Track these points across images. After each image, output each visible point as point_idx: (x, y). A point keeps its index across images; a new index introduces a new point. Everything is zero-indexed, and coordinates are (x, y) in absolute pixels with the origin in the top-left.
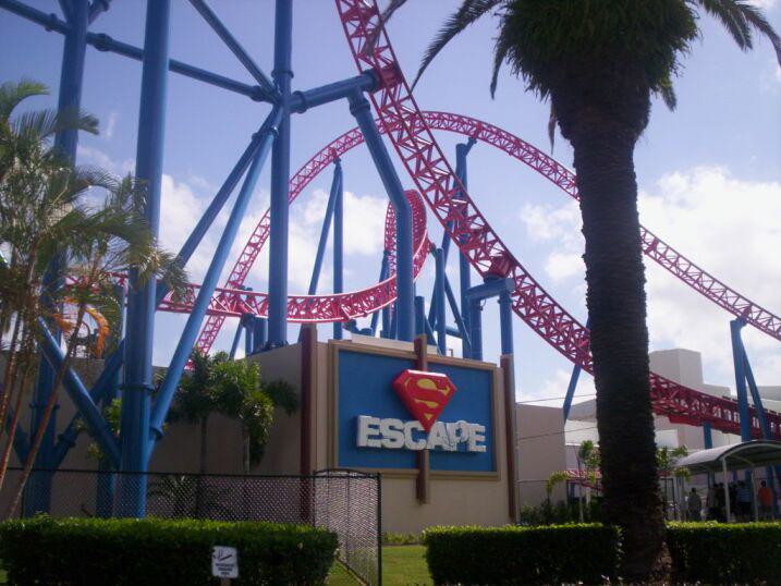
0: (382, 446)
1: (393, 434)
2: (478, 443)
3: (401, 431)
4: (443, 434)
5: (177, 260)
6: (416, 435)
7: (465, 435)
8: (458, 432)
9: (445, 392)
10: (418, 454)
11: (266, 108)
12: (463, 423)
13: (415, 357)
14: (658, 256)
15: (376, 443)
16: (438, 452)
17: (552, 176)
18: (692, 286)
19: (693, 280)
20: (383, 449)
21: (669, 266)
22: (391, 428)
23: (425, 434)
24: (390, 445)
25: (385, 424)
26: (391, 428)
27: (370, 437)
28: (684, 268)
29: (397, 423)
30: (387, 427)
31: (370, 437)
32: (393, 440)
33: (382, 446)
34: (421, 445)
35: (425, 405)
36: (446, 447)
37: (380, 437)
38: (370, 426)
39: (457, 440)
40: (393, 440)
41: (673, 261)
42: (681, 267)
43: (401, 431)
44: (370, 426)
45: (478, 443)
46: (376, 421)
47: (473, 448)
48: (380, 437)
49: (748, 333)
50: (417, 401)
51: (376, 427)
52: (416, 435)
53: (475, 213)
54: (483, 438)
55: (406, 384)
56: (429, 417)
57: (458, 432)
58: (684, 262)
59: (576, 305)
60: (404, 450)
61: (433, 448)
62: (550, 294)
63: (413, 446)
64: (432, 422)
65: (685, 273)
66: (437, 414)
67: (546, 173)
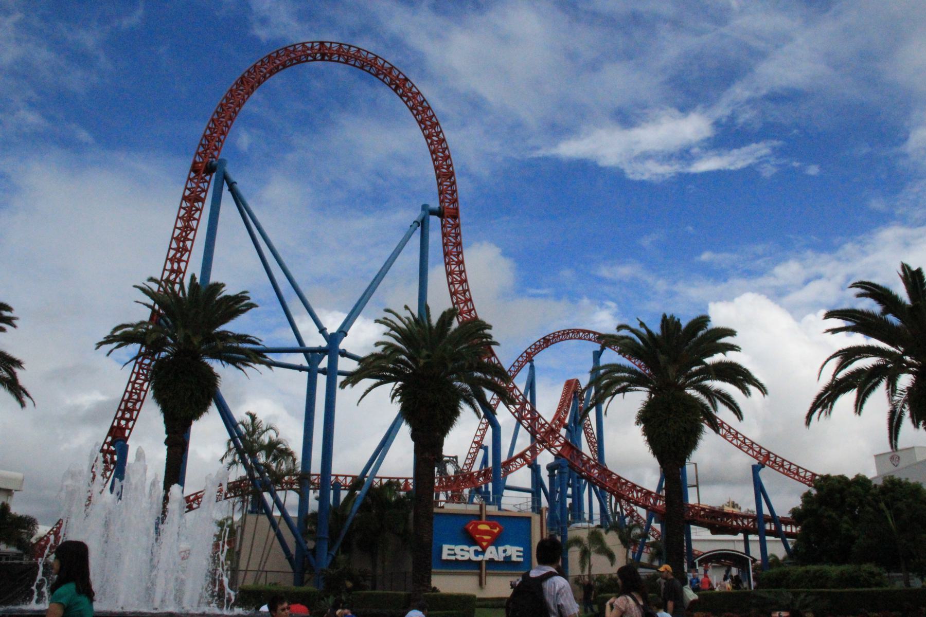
0: (456, 559)
1: (463, 553)
2: (518, 556)
3: (468, 551)
4: (492, 553)
5: (592, 606)
6: (477, 553)
7: (508, 553)
8: (505, 551)
9: (496, 531)
10: (480, 563)
11: (324, 344)
12: (508, 547)
13: (478, 513)
14: (771, 463)
15: (453, 558)
16: (491, 562)
17: (735, 442)
18: (793, 478)
19: (794, 473)
20: (456, 560)
21: (793, 476)
22: (462, 550)
23: (483, 552)
24: (459, 558)
25: (457, 549)
26: (462, 550)
27: (449, 555)
28: (802, 475)
29: (466, 547)
30: (459, 550)
31: (449, 555)
32: (462, 556)
33: (456, 559)
34: (480, 558)
35: (483, 538)
36: (496, 559)
37: (455, 554)
38: (449, 549)
39: (504, 555)
40: (462, 556)
41: (795, 472)
42: (785, 467)
43: (468, 551)
44: (449, 549)
45: (518, 556)
46: (452, 547)
47: (514, 559)
48: (455, 554)
49: (766, 474)
50: (477, 536)
51: (453, 550)
52: (477, 553)
53: (176, 230)
54: (521, 554)
55: (471, 528)
56: (485, 544)
57: (505, 551)
58: (802, 470)
59: (521, 426)
60: (470, 560)
61: (488, 559)
62: (140, 413)
63: (474, 558)
64: (487, 546)
65: (804, 477)
66: (491, 543)
67: (730, 439)
